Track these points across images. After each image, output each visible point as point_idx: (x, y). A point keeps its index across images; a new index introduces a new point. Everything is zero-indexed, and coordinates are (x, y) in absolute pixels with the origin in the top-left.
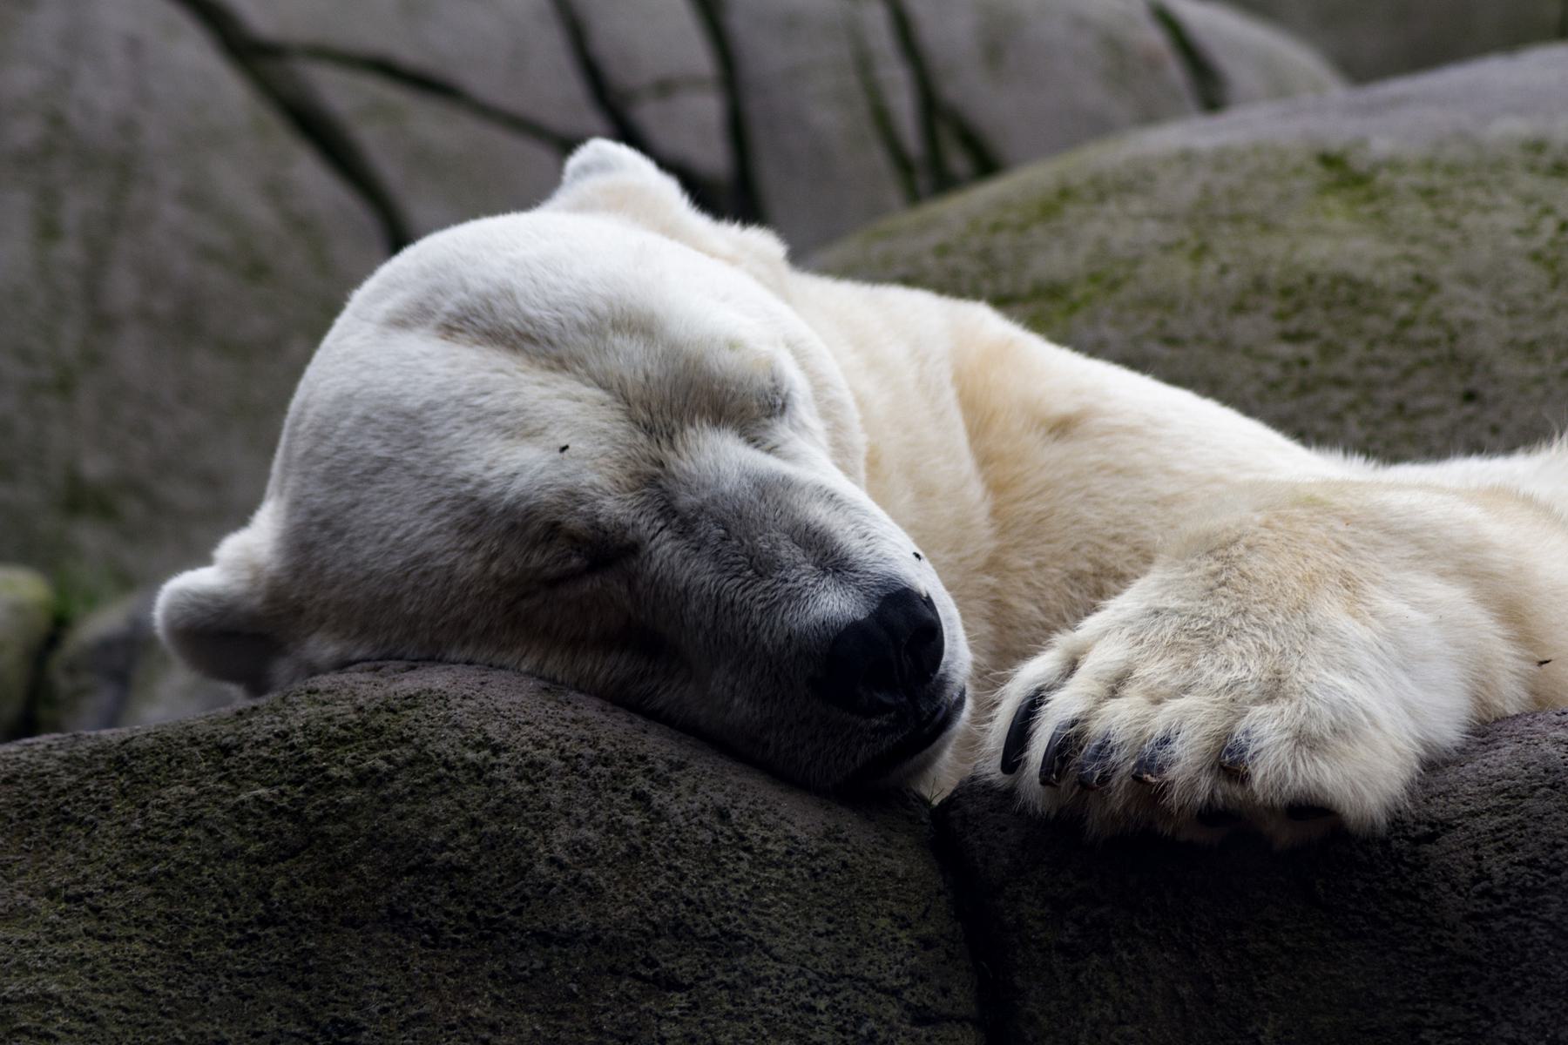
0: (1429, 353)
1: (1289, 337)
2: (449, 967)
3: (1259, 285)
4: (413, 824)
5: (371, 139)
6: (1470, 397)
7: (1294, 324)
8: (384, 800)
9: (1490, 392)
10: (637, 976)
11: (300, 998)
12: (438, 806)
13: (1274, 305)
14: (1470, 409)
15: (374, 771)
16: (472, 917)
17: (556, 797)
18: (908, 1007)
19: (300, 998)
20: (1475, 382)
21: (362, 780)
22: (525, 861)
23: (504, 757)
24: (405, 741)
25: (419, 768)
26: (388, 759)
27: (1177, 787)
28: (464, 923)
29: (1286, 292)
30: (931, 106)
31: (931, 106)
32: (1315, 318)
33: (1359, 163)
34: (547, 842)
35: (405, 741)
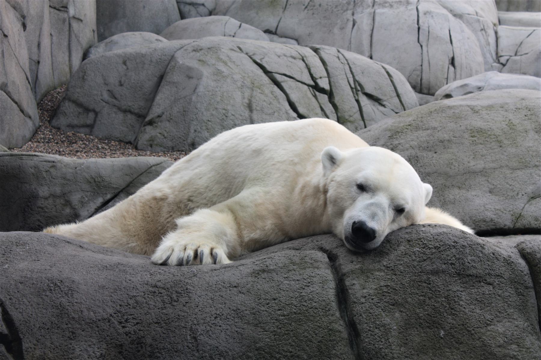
0: (494, 140)
1: (472, 137)
2: (453, 281)
3: (467, 129)
4: (445, 256)
5: (284, 85)
6: (501, 146)
7: (473, 135)
8: (439, 252)
9: (504, 146)
10: (484, 282)
11: (429, 286)
12: (448, 253)
13: (470, 132)
14: (501, 148)
15: (437, 246)
16: (456, 272)
17: (468, 251)
18: (525, 286)
19: (429, 286)
20: (501, 144)
21: (435, 248)
22: (464, 263)
23: (458, 244)
24: (441, 241)
25: (444, 246)
26: (439, 245)
27: (90, 58)
28: (455, 273)
29: (471, 130)
30: (355, 81)
31: (355, 81)
32: (476, 134)
33: (476, 108)
34: (467, 259)
35: (441, 241)
